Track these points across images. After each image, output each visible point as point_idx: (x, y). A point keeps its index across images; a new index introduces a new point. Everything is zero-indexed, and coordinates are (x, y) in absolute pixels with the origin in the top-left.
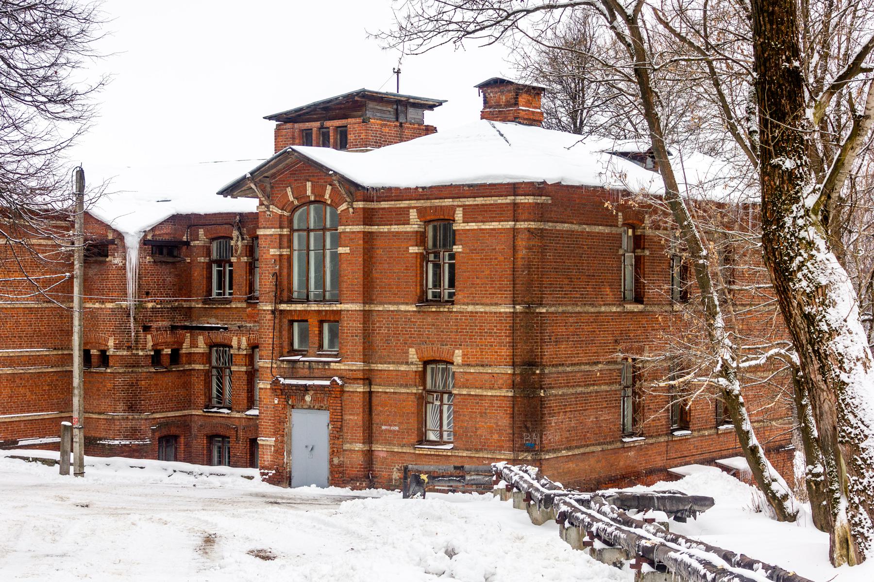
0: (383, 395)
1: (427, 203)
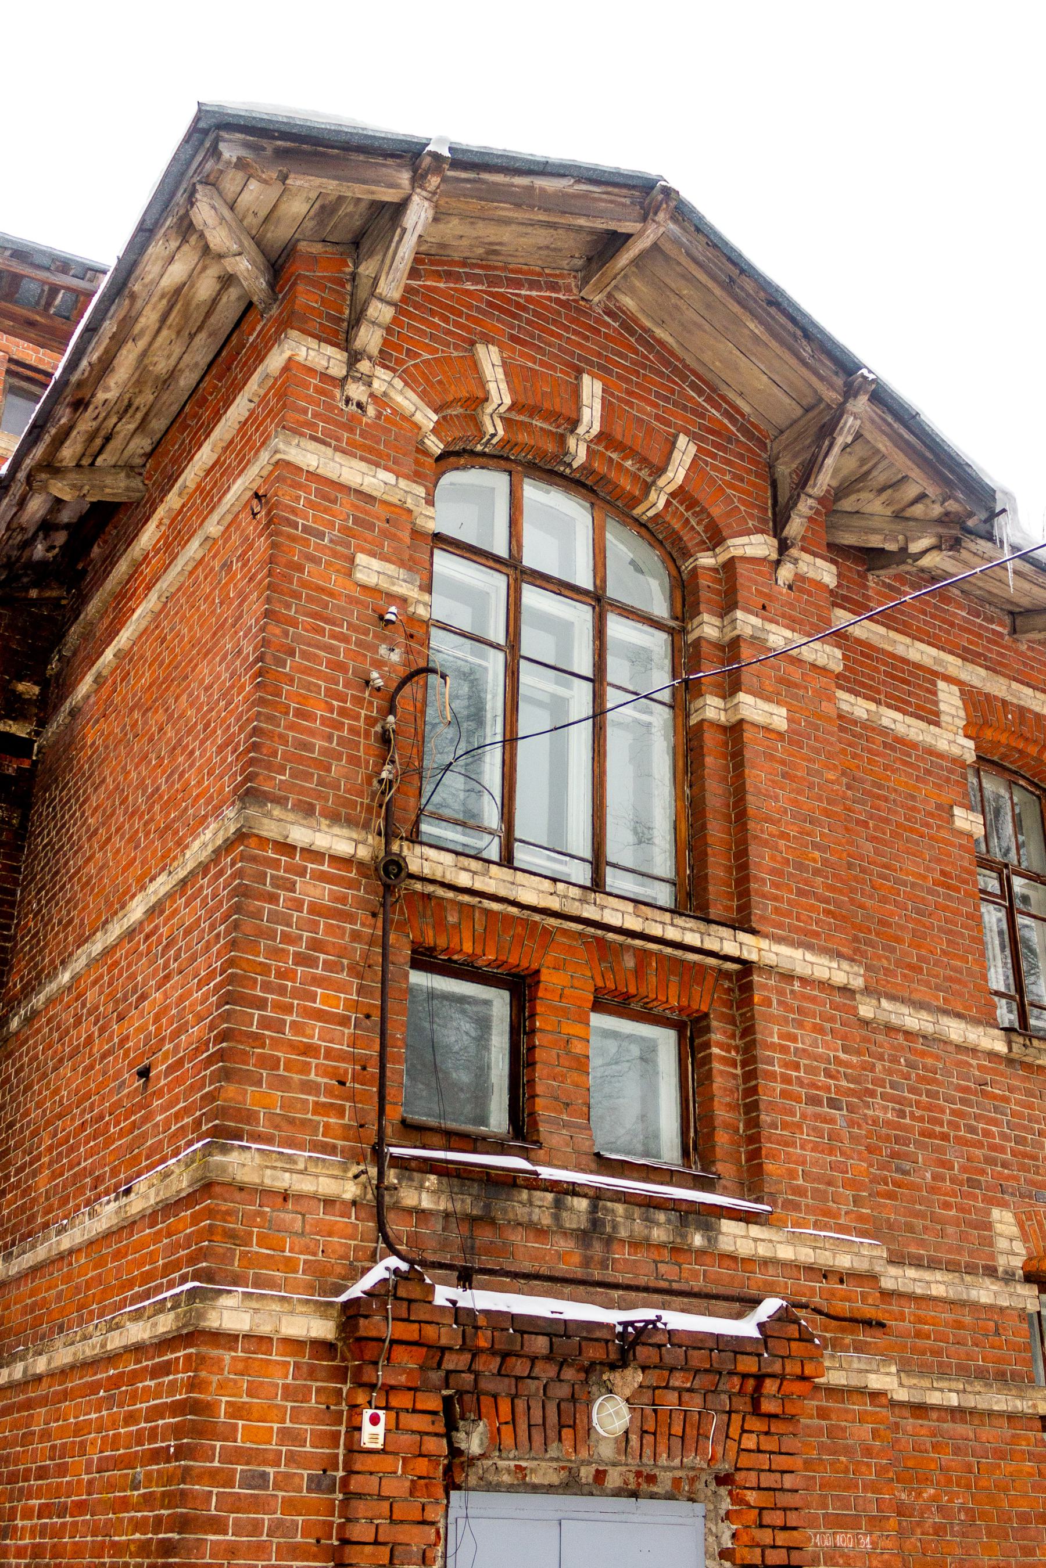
0: (910, 1423)
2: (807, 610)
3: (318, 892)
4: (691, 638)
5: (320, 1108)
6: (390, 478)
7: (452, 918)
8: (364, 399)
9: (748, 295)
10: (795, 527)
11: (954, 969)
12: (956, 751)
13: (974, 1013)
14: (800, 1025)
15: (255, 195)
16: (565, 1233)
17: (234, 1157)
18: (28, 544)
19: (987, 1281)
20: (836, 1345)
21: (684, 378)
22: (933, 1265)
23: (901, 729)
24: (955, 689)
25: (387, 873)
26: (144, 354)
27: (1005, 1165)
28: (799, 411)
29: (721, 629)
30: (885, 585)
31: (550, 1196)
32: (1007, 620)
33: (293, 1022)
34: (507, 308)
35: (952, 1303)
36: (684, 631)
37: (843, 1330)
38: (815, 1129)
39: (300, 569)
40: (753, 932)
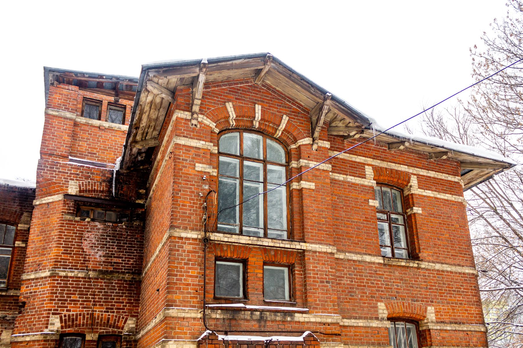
1: (384, 165)
2: (322, 156)
3: (189, 247)
4: (290, 167)
5: (191, 298)
6: (204, 142)
7: (225, 248)
8: (196, 123)
9: (295, 78)
10: (316, 134)
11: (369, 243)
12: (370, 184)
13: (374, 253)
14: (318, 264)
15: (163, 81)
16: (254, 320)
17: (171, 311)
18: (137, 157)
19: (375, 321)
20: (322, 340)
21: (285, 99)
22: (360, 318)
23: (353, 181)
24: (371, 167)
25: (205, 242)
26: (149, 115)
27: (382, 291)
28: (316, 104)
29: (297, 164)
30: (349, 142)
31: (250, 312)
32: (387, 145)
33: (184, 279)
34: (234, 91)
35: (365, 327)
36: (289, 165)
37: (329, 337)
38: (322, 289)
39: (182, 170)
40: (305, 242)
